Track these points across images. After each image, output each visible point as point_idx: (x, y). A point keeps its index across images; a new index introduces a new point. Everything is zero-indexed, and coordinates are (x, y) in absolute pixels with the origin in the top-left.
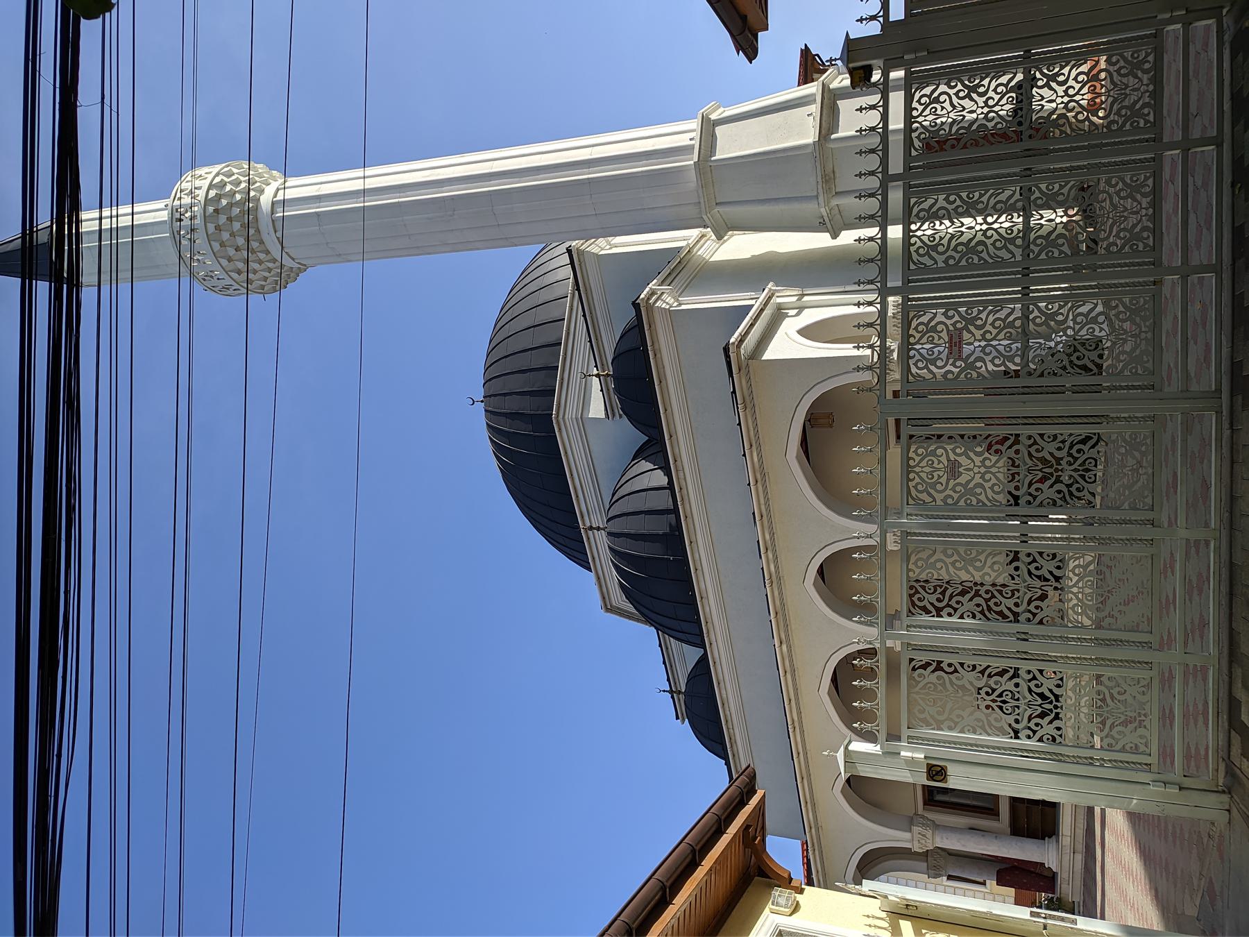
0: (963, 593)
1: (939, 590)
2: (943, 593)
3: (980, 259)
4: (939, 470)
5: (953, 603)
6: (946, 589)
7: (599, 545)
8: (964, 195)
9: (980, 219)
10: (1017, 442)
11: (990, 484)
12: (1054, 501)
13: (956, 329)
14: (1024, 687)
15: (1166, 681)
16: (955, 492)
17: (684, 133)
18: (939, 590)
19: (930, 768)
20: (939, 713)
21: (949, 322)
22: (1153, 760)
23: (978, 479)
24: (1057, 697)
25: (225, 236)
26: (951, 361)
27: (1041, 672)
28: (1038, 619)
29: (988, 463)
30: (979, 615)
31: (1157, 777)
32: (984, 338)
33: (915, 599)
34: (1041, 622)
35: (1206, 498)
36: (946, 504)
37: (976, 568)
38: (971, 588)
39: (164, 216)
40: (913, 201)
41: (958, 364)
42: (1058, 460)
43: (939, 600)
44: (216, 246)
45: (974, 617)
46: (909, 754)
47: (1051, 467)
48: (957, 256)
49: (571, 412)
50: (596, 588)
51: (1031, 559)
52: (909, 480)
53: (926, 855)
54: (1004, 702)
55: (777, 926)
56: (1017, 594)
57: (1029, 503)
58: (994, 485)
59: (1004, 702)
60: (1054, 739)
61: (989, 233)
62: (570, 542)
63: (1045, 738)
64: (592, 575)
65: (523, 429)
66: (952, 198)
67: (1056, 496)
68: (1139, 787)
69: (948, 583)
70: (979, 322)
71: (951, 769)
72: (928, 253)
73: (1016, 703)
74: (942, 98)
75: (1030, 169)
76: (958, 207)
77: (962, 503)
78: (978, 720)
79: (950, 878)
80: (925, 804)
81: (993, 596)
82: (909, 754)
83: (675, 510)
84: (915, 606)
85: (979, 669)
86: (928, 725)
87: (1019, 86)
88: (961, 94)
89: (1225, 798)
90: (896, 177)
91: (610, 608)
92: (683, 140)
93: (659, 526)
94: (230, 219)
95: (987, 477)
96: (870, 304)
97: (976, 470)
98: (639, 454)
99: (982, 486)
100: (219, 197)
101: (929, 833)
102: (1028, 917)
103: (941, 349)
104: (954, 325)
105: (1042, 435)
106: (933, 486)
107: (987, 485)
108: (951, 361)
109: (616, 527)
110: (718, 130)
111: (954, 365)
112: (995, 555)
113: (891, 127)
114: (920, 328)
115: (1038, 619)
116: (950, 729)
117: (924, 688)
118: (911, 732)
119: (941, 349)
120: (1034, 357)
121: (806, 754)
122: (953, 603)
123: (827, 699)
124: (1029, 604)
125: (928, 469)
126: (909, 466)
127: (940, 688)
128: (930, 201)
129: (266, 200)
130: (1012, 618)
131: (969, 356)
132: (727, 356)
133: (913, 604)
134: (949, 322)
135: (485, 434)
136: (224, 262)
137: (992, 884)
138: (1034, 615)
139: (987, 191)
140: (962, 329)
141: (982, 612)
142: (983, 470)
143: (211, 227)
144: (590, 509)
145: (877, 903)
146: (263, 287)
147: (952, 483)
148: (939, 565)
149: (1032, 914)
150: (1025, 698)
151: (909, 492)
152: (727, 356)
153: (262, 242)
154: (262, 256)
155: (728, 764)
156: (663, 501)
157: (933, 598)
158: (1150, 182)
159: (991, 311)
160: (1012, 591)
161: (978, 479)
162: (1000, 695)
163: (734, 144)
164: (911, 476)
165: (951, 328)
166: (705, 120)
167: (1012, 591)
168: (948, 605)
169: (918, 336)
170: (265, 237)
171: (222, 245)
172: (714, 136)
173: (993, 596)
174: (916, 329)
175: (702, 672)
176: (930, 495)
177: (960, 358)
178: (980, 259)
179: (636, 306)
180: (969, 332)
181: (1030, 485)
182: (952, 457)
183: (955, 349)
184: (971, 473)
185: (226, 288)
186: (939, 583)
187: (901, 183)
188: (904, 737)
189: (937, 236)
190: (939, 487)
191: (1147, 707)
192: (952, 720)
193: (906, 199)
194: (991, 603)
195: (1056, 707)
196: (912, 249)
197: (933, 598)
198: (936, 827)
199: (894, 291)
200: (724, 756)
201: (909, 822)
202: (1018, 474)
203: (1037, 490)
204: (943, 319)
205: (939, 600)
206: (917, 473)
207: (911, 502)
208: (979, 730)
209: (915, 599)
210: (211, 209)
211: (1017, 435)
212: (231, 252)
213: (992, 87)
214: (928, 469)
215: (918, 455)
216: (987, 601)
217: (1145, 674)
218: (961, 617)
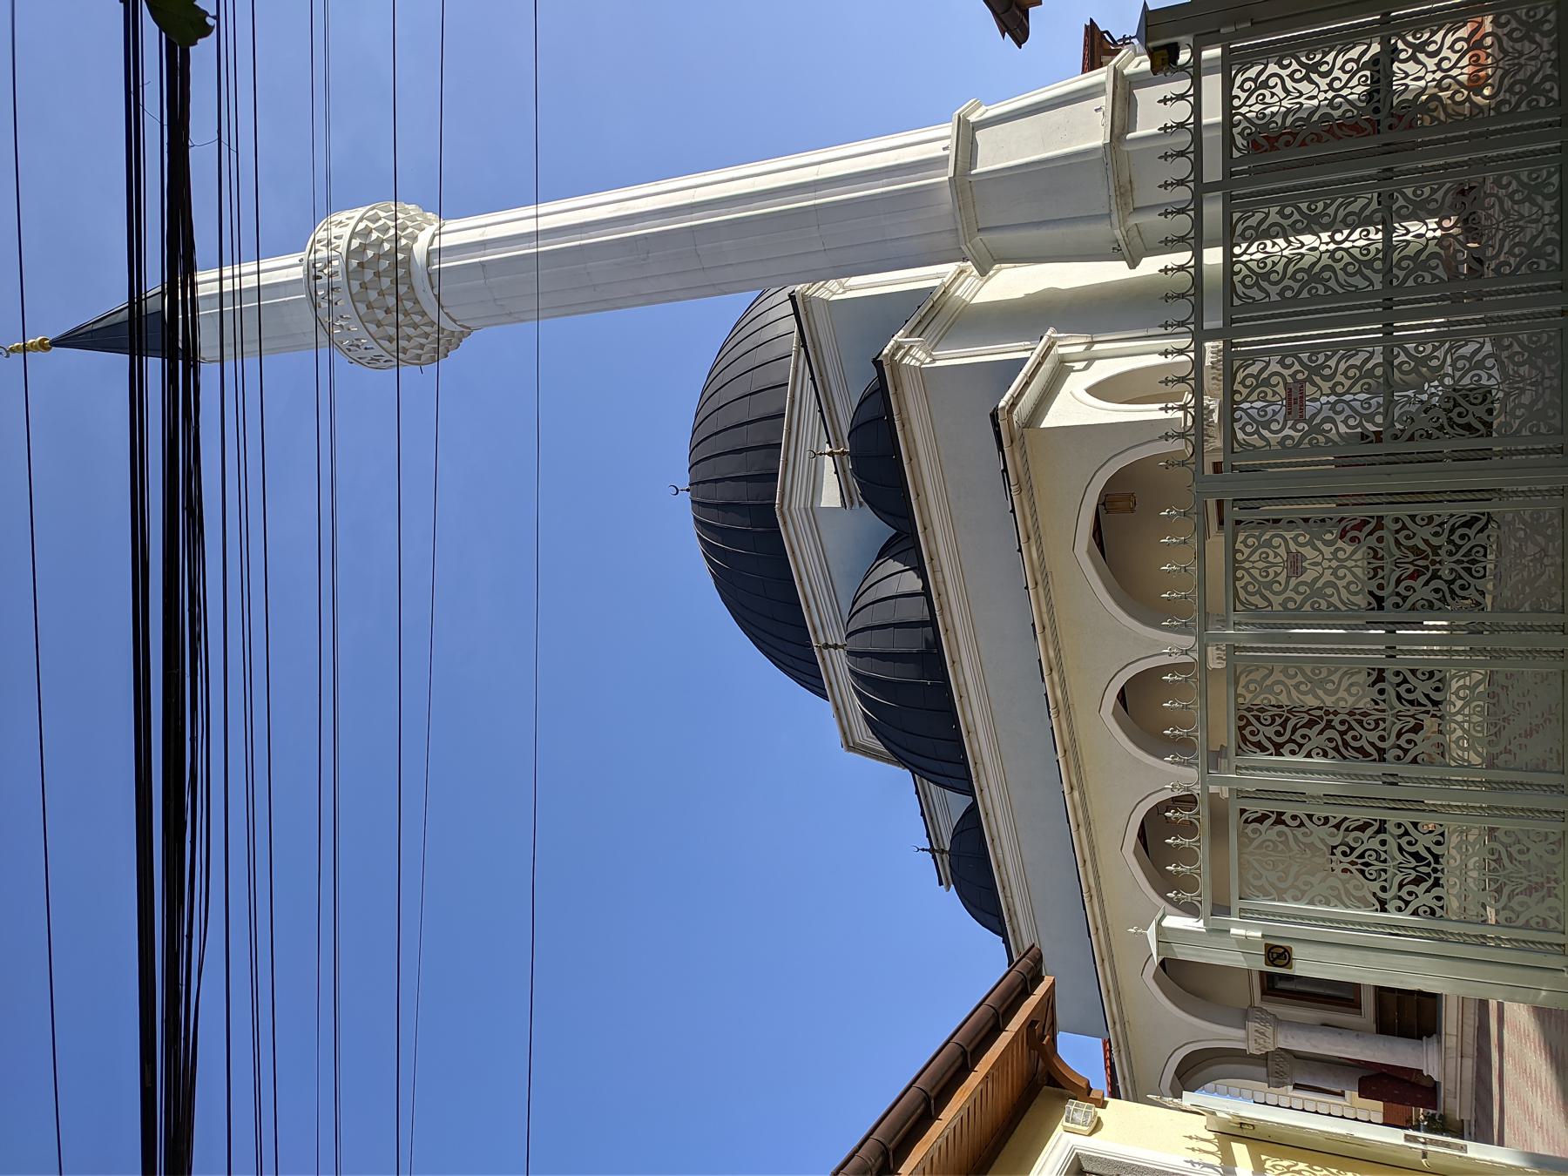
0: (1311, 724)
1: (1278, 721)
2: (1284, 725)
3: (1327, 288)
4: (1275, 565)
5: (1297, 737)
6: (1288, 719)
7: (837, 667)
8: (1304, 206)
9: (1325, 236)
11: (1344, 582)
13: (1296, 381)
14: (1392, 845)
16: (1298, 593)
17: (936, 141)
18: (1278, 721)
19: (1270, 949)
21: (1286, 372)
23: (1328, 576)
24: (1437, 858)
25: (373, 295)
26: (1290, 423)
27: (1415, 825)
28: (1409, 603)
29: (1341, 555)
30: (1331, 753)
32: (1333, 392)
33: (1246, 732)
36: (1286, 609)
37: (1327, 692)
38: (1321, 718)
39: (298, 273)
40: (1236, 216)
41: (1300, 426)
42: (1435, 549)
44: (362, 308)
45: (1325, 755)
46: (1242, 932)
47: (1426, 558)
48: (1296, 286)
49: (798, 501)
50: (835, 721)
52: (1236, 579)
53: (1264, 1059)
54: (1367, 864)
55: (1073, 1149)
56: (1382, 725)
59: (1367, 864)
60: (1433, 912)
61: (1338, 255)
62: (808, 674)
63: (1418, 606)
64: (829, 704)
65: (737, 523)
66: (1288, 211)
67: (1432, 596)
68: (1548, 974)
69: (1290, 711)
70: (1327, 372)
71: (1298, 951)
72: (1257, 432)
73: (1382, 866)
74: (1274, 380)
75: (1390, 170)
76: (1296, 222)
77: (1307, 607)
78: (1333, 888)
79: (1297, 1087)
80: (1263, 993)
81: (1351, 728)
82: (1242, 932)
83: (933, 623)
84: (1246, 741)
85: (1333, 822)
86: (1266, 895)
87: (1375, 60)
88: (1298, 76)
90: (1213, 186)
91: (852, 746)
92: (935, 150)
93: (912, 642)
94: (377, 274)
95: (1341, 573)
96: (1181, 352)
97: (1326, 564)
99: (1335, 586)
100: (363, 248)
101: (1269, 1031)
102: (1401, 1142)
103: (1277, 408)
104: (1293, 376)
105: (1413, 517)
106: (1269, 586)
107: (1341, 584)
108: (1290, 423)
110: (979, 135)
111: (1293, 428)
112: (1353, 674)
113: (1205, 121)
116: (1296, 899)
117: (1260, 846)
118: (1245, 904)
119: (1277, 408)
121: (1106, 930)
122: (1297, 737)
123: (1132, 861)
125: (1261, 565)
126: (1235, 560)
127: (1281, 847)
129: (420, 249)
130: (1376, 755)
131: (1314, 416)
132: (996, 425)
133: (1243, 736)
134: (1286, 372)
135: (692, 530)
136: (372, 328)
137: (1352, 1095)
138: (1406, 751)
139: (1337, 670)
140: (1304, 381)
141: (1336, 749)
142: (1334, 564)
143: (355, 285)
144: (824, 620)
145: (1202, 1120)
146: (419, 357)
147: (1293, 582)
148: (1277, 688)
149: (1407, 1138)
150: (1394, 859)
151: (1236, 595)
152: (996, 425)
153: (416, 301)
154: (417, 318)
155: (1006, 941)
156: (915, 611)
157: (1270, 732)
158: (1555, 179)
159: (1345, 673)
160: (1377, 722)
161: (1328, 576)
162: (1362, 856)
163: (999, 152)
164: (1239, 574)
165: (1290, 380)
166: (962, 123)
167: (1377, 722)
168: (1291, 741)
169: (1247, 551)
170: (421, 296)
171: (369, 306)
172: (973, 144)
173: (1351, 728)
174: (1241, 87)
176: (1261, 289)
177: (1302, 419)
178: (1327, 288)
180: (1314, 384)
181: (1398, 582)
182: (1293, 547)
183: (1296, 407)
184: (1319, 569)
185: (376, 359)
186: (1278, 711)
188: (1235, 910)
190: (1276, 587)
192: (1294, 741)
193: (1227, 215)
194: (1348, 737)
195: (1433, 562)
196: (1236, 279)
197: (1270, 732)
198: (1278, 1022)
199: (1213, 335)
200: (1002, 932)
201: (1244, 1016)
202: (1382, 568)
204: (1278, 368)
205: (1278, 734)
206: (1247, 570)
209: (1246, 732)
210: (354, 263)
211: (1380, 518)
212: (381, 315)
213: (1339, 63)
214: (1261, 565)
215: (1247, 546)
216: (1342, 733)
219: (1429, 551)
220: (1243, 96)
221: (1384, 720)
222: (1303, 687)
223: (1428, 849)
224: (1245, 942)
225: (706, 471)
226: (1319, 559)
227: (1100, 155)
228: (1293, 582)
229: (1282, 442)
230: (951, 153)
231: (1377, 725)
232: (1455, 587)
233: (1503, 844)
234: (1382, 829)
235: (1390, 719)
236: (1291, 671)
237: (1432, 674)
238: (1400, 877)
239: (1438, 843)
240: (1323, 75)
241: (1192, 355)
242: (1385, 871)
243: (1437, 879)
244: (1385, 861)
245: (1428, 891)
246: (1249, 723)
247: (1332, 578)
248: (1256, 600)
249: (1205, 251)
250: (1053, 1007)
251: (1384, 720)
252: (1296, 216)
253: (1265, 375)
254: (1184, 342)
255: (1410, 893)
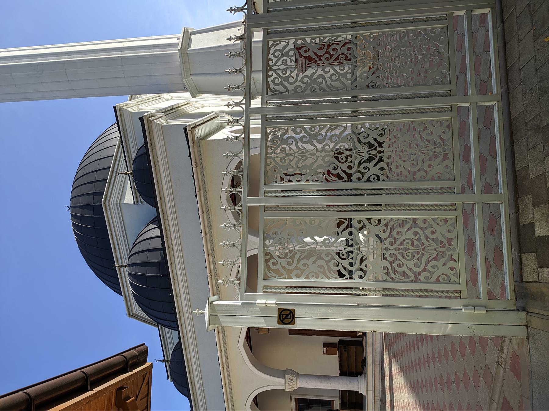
2: (292, 258)
4: (291, 66)
5: (300, 266)
7: (124, 277)
10: (350, 225)
12: (378, 176)
15: (467, 215)
16: (303, 82)
17: (175, 39)
19: (281, 312)
20: (289, 263)
22: (462, 287)
24: (380, 144)
31: (466, 302)
33: (270, 264)
34: (368, 180)
35: (500, 265)
36: (296, 92)
40: (270, 43)
43: (289, 263)
46: (264, 302)
47: (375, 149)
49: (113, 200)
51: (361, 225)
56: (350, 159)
57: (359, 179)
58: (332, 75)
60: (379, 178)
63: (371, 179)
64: (123, 298)
65: (87, 213)
68: (452, 312)
70: (320, 137)
71: (298, 313)
75: (356, 111)
77: (308, 91)
78: (321, 266)
83: (163, 249)
86: (280, 275)
89: (523, 314)
91: (131, 315)
92: (175, 41)
93: (156, 257)
96: (238, 104)
97: (318, 154)
98: (152, 222)
105: (369, 220)
107: (327, 76)
109: (134, 260)
110: (193, 37)
112: (333, 129)
114: (277, 54)
115: (366, 177)
116: (298, 276)
118: (267, 283)
120: (362, 74)
121: (230, 385)
124: (359, 167)
125: (282, 155)
126: (268, 65)
128: (284, 44)
130: (346, 178)
132: (186, 134)
139: (325, 126)
144: (121, 255)
147: (301, 76)
151: (268, 86)
152: (186, 134)
156: (157, 244)
159: (329, 129)
163: (199, 43)
164: (269, 161)
168: (297, 268)
169: (275, 59)
172: (190, 39)
174: (274, 54)
175: (178, 348)
176: (284, 86)
179: (141, 119)
181: (360, 164)
184: (315, 157)
187: (262, 28)
188: (262, 191)
189: (287, 159)
191: (454, 243)
193: (265, 41)
195: (380, 152)
200: (188, 396)
203: (366, 168)
206: (275, 71)
207: (270, 93)
208: (321, 276)
211: (351, 220)
214: (283, 67)
215: (275, 56)
217: (450, 215)
218: (308, 278)
219: (377, 145)
220: (275, 59)
221: (351, 156)
222: (305, 140)
223: (375, 140)
224: (265, 308)
225: (77, 192)
226: (315, 151)
227: (239, 47)
228: (301, 76)
229: (295, 90)
230: (180, 42)
231: (347, 159)
232: (395, 265)
233: (421, 228)
234: (350, 225)
235: (354, 155)
236: (298, 130)
237: (380, 221)
238: (359, 158)
239: (380, 135)
240: (320, 142)
241: (244, 106)
242: (352, 252)
243: (381, 157)
244: (351, 246)
245: (376, 165)
246: (272, 257)
247: (322, 73)
248: (280, 88)
249: (251, 101)
250: (149, 383)
251: (351, 156)
252: (303, 134)
253: (286, 50)
254: (238, 99)
255: (366, 168)
